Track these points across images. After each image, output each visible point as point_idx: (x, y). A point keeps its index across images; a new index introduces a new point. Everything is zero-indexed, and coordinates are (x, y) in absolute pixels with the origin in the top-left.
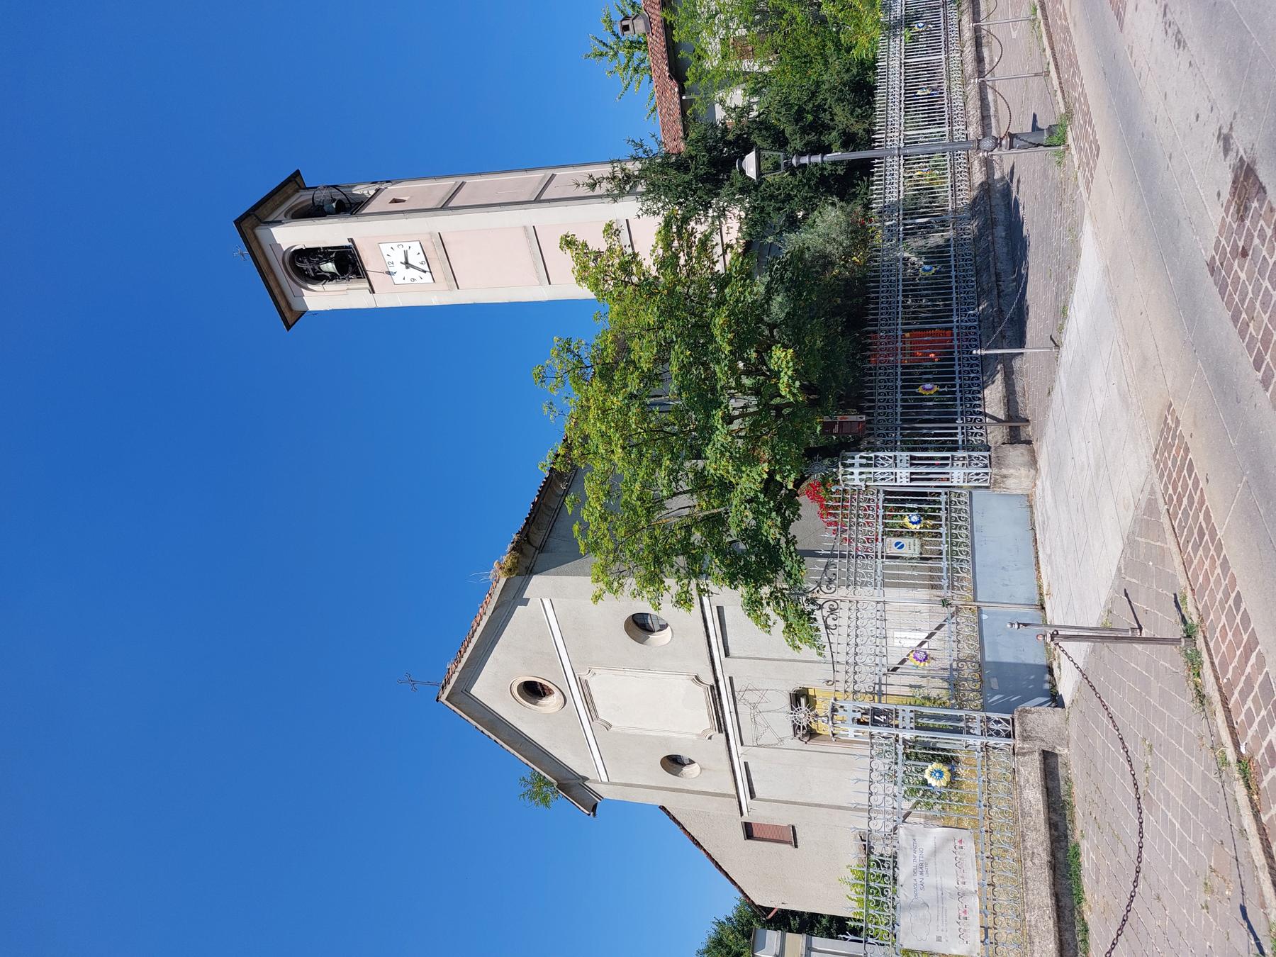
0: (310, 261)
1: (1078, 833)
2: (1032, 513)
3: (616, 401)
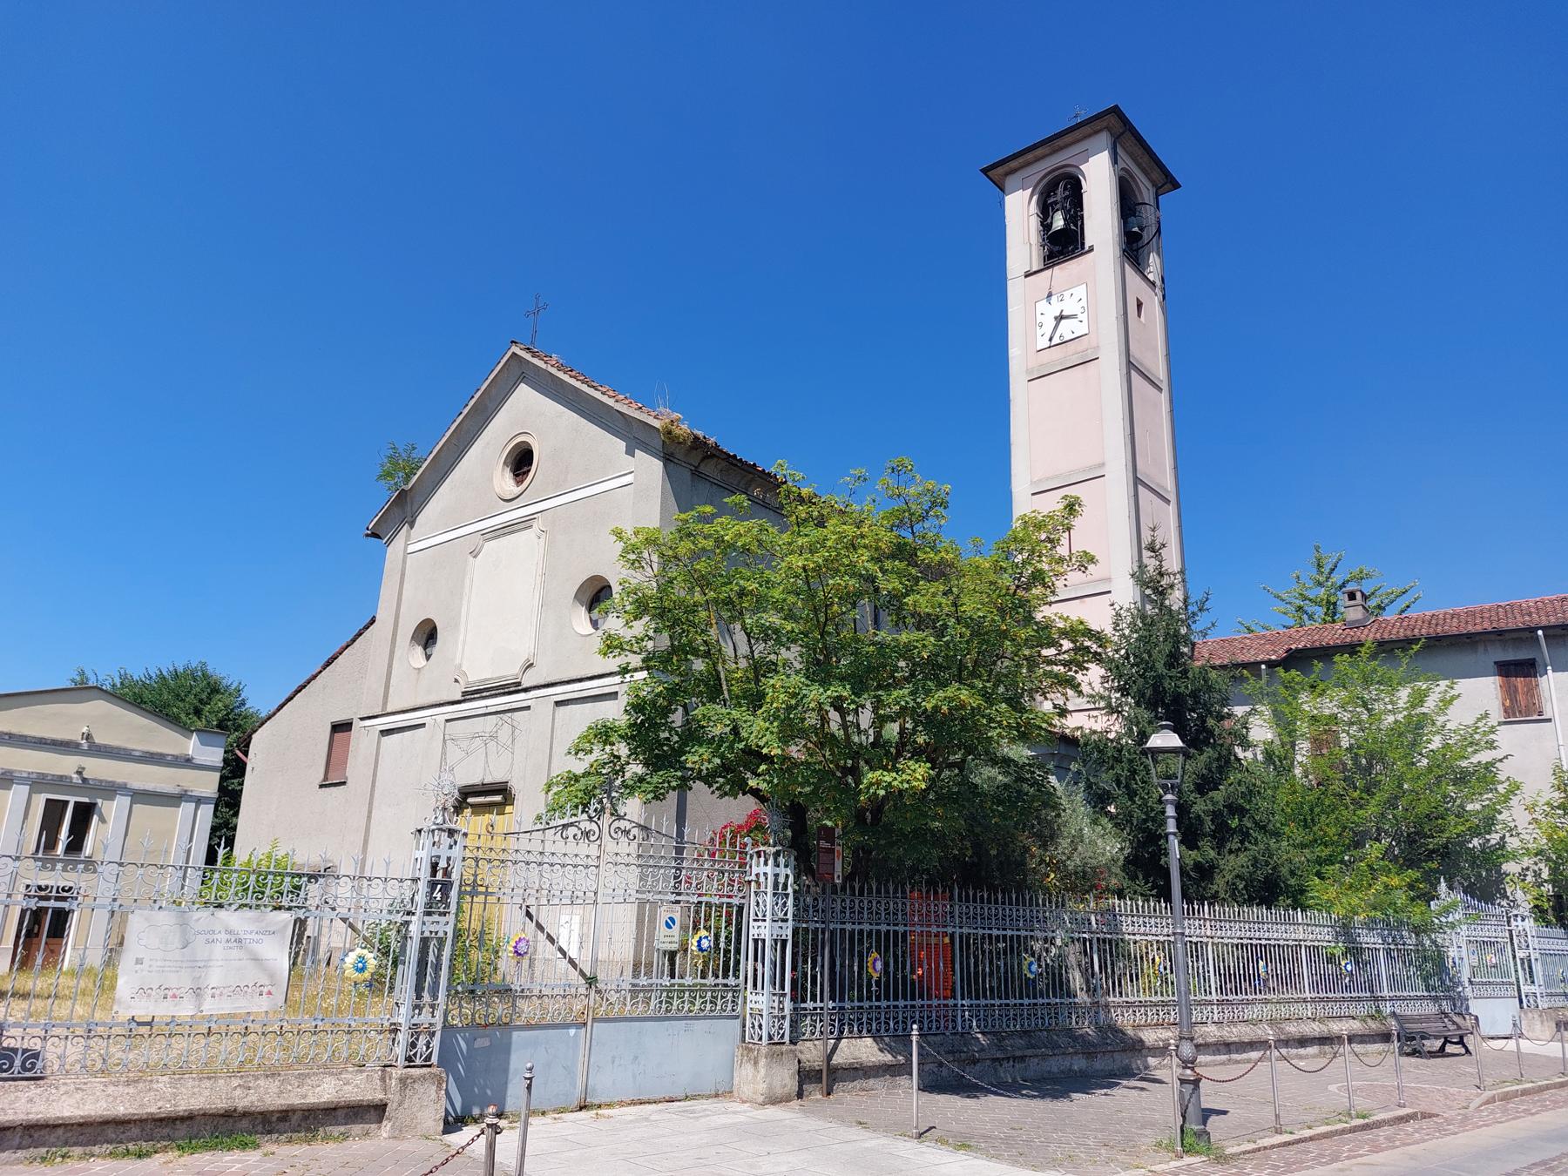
0: (1066, 198)
1: (273, 1148)
2: (709, 1097)
3: (863, 559)
